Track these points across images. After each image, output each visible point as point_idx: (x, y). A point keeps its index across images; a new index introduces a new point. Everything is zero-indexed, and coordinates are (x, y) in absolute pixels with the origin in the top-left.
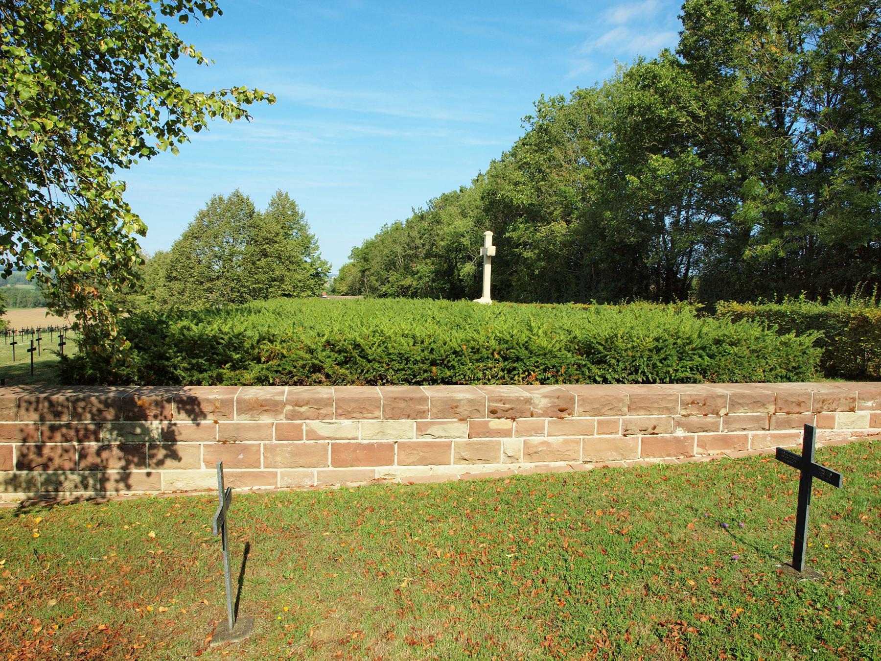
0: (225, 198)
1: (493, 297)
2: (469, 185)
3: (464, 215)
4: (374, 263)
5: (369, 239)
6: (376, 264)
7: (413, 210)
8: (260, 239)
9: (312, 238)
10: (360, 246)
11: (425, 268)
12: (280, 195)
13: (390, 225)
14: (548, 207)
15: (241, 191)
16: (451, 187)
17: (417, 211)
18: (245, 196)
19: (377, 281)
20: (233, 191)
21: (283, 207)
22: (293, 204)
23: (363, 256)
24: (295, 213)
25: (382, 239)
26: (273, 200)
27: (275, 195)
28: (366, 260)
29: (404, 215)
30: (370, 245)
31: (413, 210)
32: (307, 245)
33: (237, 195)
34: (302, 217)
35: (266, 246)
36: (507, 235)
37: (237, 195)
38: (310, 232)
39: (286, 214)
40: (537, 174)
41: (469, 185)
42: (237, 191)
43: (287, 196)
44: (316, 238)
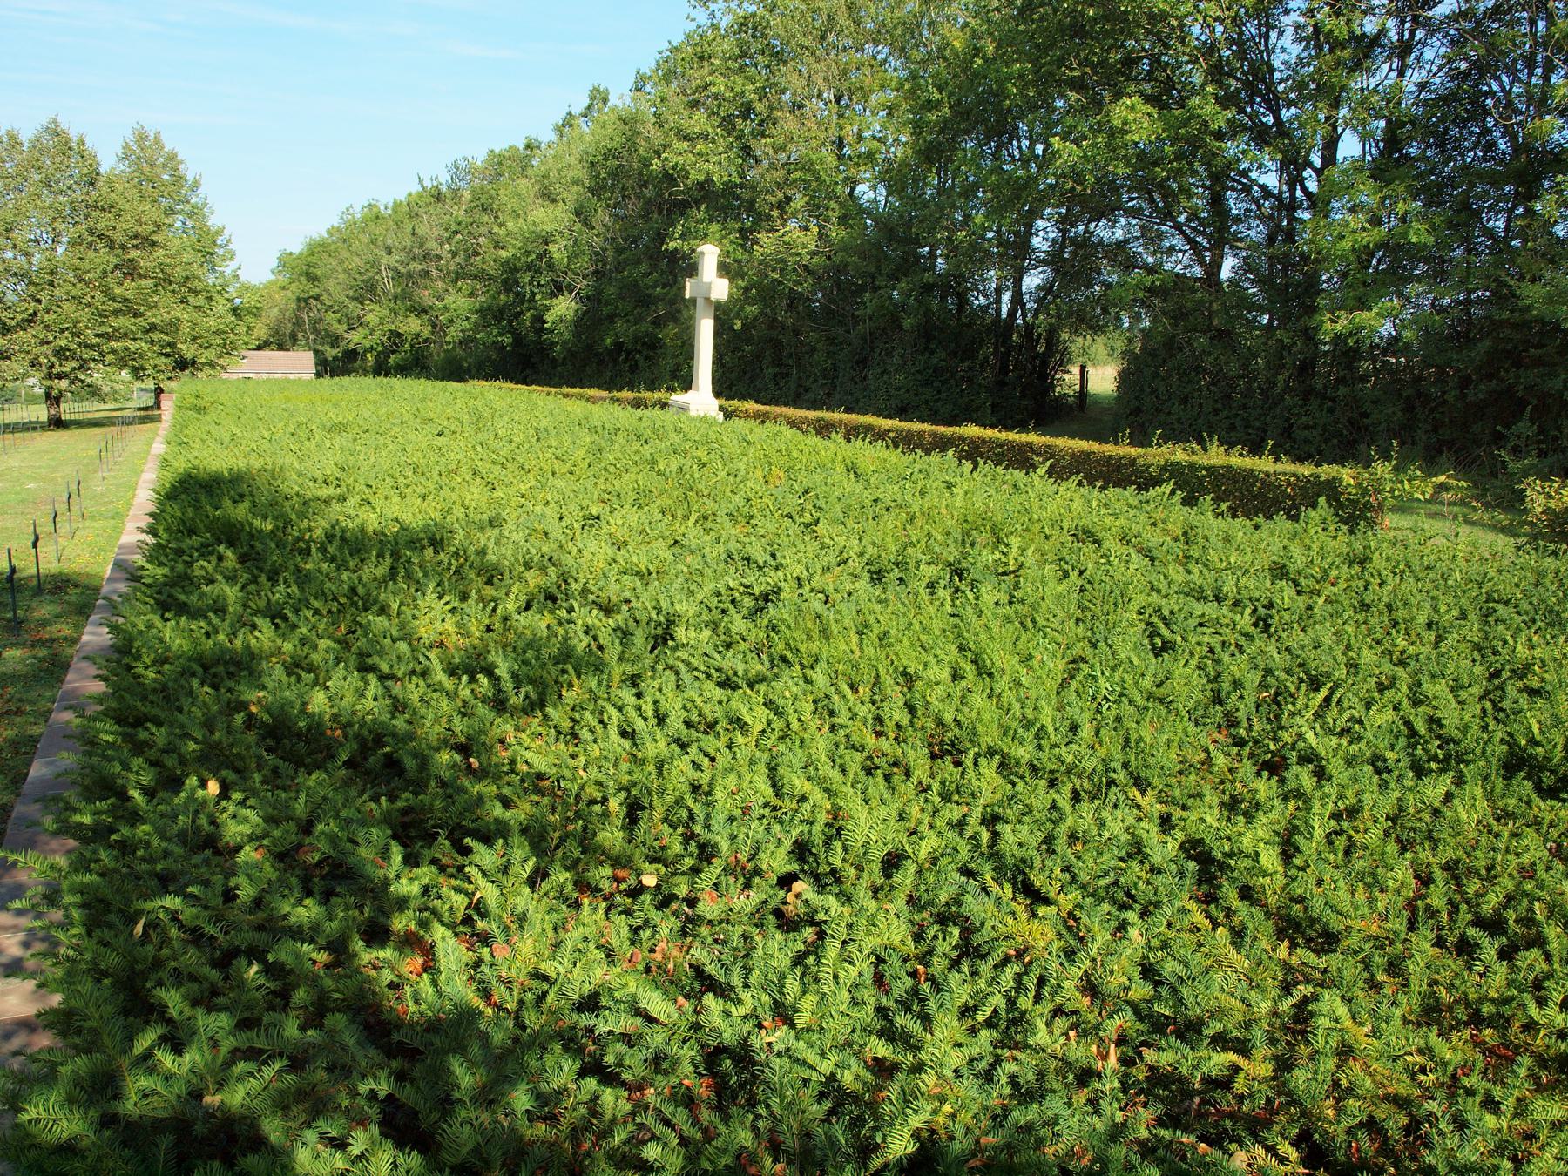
0: (26, 136)
1: (722, 388)
2: (547, 136)
3: (547, 196)
4: (331, 285)
5: (316, 236)
6: (336, 288)
7: (421, 182)
8: (119, 238)
9: (219, 232)
10: (297, 247)
11: (459, 305)
12: (141, 137)
13: (358, 208)
14: (772, 193)
15: (63, 126)
16: (511, 138)
17: (428, 184)
18: (74, 136)
19: (339, 321)
20: (45, 122)
21: (152, 165)
22: (172, 157)
23: (305, 269)
24: (178, 180)
25: (344, 237)
26: (127, 146)
27: (130, 138)
28: (312, 278)
29: (392, 187)
30: (317, 249)
31: (421, 182)
32: (208, 247)
33: (54, 130)
34: (195, 186)
35: (134, 254)
36: (672, 245)
37: (54, 130)
38: (214, 222)
39: (156, 173)
40: (743, 122)
41: (547, 136)
42: (55, 122)
43: (157, 140)
44: (226, 233)
